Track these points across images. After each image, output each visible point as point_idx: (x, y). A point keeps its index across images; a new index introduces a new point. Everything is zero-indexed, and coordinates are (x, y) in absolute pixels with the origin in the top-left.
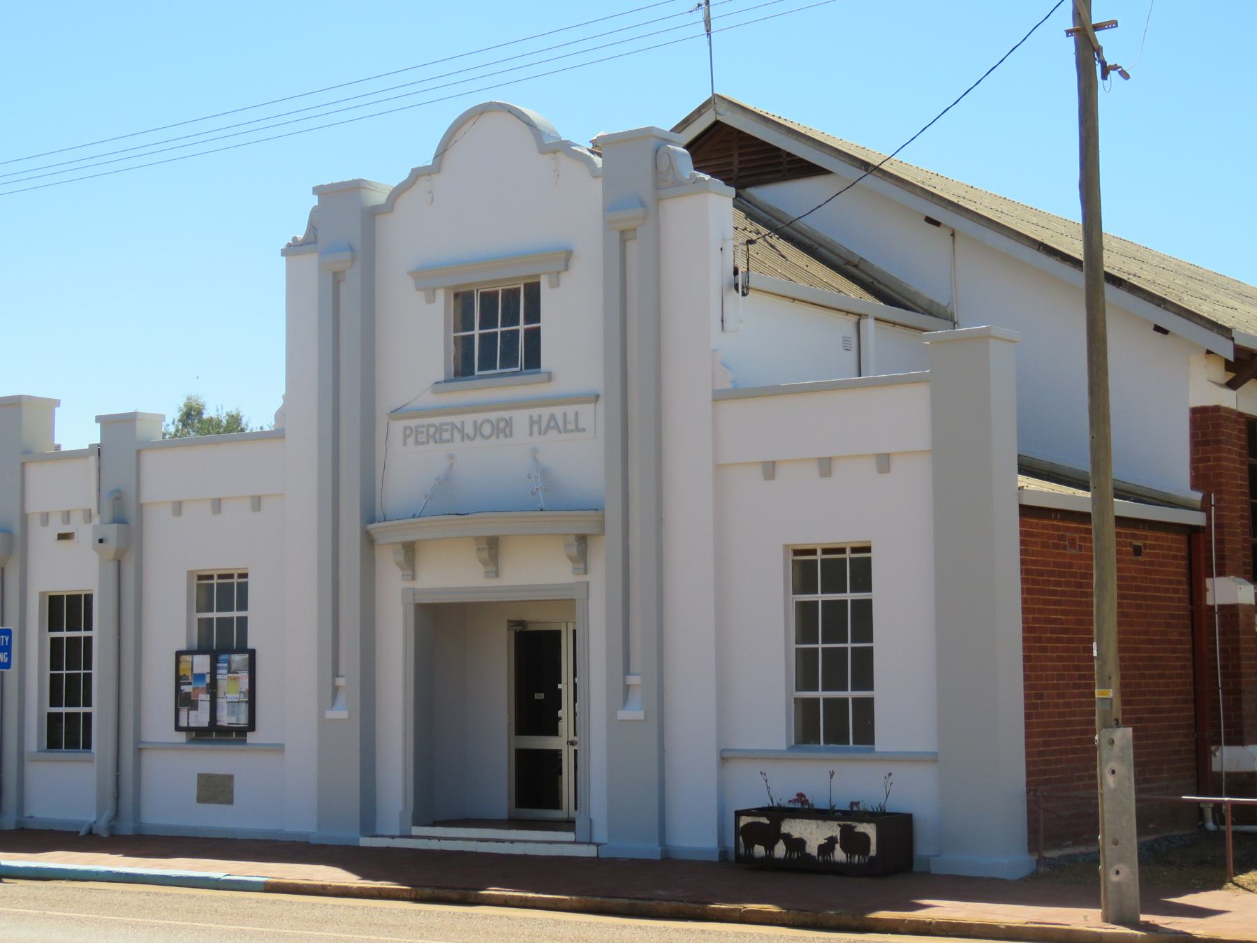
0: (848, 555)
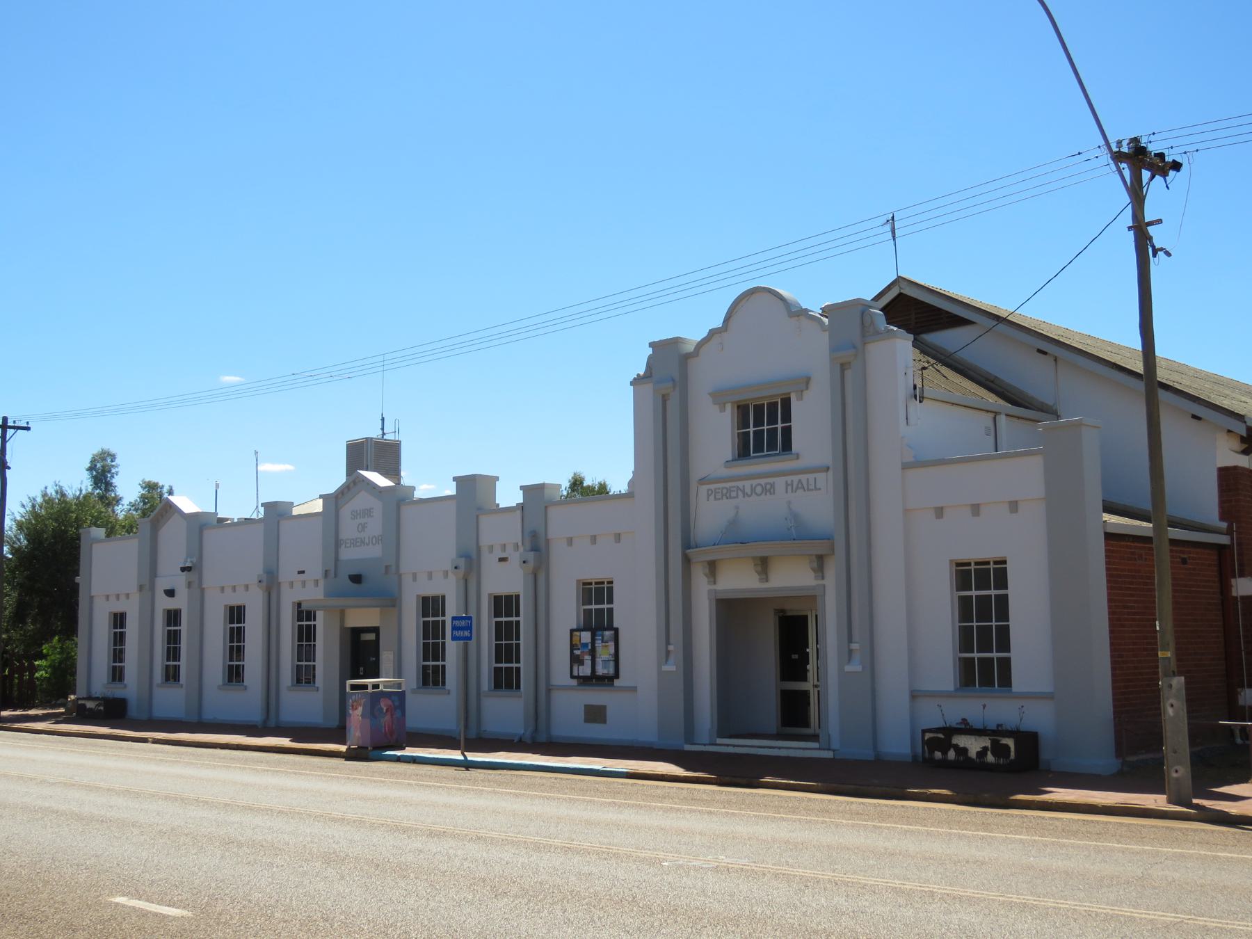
0: (992, 566)
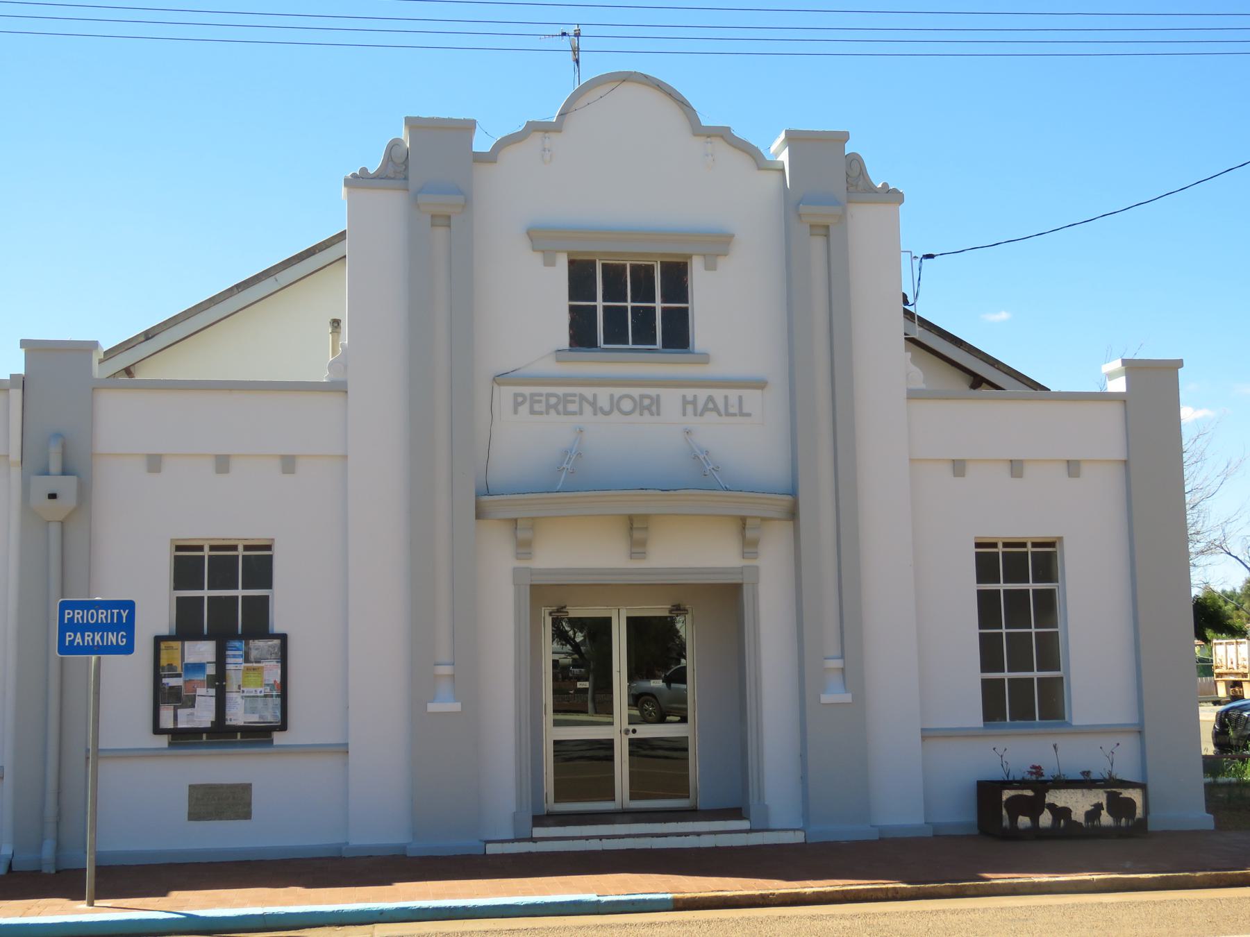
0: (1030, 549)
